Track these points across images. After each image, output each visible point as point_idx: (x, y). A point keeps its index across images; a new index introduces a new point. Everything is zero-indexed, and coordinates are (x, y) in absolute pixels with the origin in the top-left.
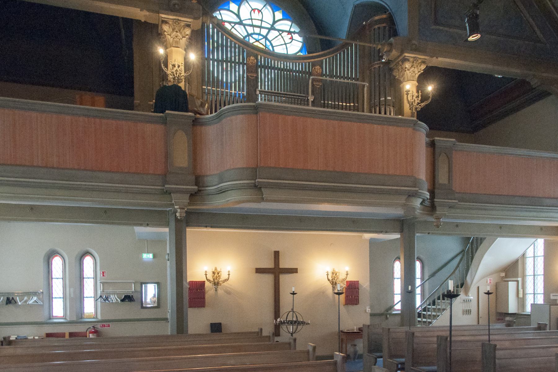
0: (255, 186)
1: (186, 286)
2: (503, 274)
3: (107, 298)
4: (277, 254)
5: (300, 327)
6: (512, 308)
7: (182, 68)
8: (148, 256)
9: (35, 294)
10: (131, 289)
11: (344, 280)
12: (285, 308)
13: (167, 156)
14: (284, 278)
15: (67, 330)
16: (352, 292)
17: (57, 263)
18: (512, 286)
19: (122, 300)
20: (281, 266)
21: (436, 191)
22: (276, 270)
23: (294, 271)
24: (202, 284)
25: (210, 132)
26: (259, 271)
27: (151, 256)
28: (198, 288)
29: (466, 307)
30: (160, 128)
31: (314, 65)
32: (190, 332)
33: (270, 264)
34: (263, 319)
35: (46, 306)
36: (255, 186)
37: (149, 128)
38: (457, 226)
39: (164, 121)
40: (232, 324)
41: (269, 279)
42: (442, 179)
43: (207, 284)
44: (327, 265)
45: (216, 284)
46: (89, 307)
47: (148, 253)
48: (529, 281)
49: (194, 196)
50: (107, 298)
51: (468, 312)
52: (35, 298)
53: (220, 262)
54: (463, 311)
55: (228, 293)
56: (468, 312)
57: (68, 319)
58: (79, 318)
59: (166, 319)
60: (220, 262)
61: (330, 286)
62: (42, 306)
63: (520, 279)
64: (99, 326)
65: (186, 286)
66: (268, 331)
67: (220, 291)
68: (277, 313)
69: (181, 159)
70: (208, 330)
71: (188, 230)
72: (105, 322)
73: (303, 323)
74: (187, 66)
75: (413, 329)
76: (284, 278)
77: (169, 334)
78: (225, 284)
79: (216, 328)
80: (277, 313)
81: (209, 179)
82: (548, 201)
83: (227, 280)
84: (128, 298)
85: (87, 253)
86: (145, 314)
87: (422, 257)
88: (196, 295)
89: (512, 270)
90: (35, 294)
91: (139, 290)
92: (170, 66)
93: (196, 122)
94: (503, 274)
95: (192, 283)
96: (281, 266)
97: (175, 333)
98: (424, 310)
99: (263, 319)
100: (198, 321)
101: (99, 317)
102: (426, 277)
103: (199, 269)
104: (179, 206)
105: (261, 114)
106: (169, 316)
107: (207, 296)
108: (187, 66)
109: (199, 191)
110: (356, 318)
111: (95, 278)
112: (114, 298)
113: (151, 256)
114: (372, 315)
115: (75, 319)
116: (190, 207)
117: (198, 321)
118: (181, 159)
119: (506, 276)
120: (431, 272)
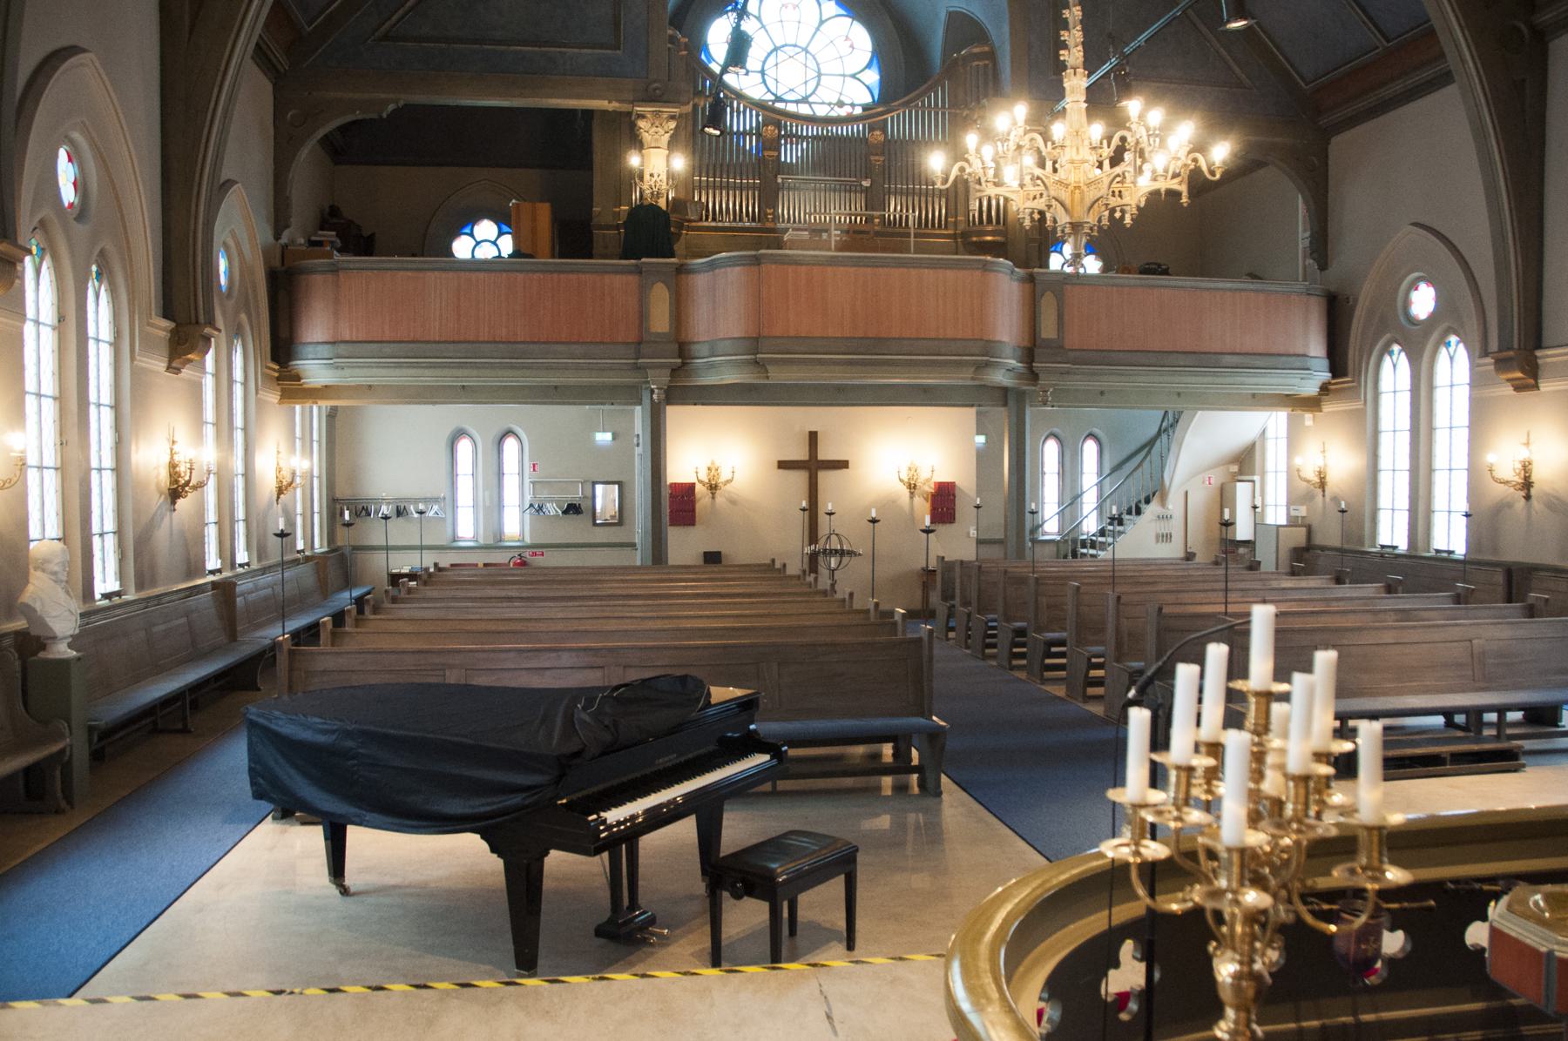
0: (756, 362)
1: (666, 493)
2: (1235, 468)
3: (540, 508)
4: (813, 437)
5: (846, 559)
6: (1243, 531)
7: (664, 177)
8: (603, 437)
9: (436, 500)
10: (577, 495)
11: (928, 480)
12: (823, 531)
13: (643, 316)
14: (825, 477)
15: (480, 559)
16: (944, 501)
17: (464, 447)
18: (1242, 491)
19: (565, 512)
20: (820, 457)
21: (1037, 351)
22: (813, 465)
23: (843, 465)
24: (692, 486)
25: (700, 281)
26: (783, 465)
27: (608, 436)
28: (685, 493)
29: (1163, 528)
30: (633, 279)
31: (872, 129)
32: (670, 562)
33: (801, 454)
34: (789, 547)
35: (449, 521)
36: (756, 362)
37: (618, 281)
38: (1102, 393)
39: (638, 271)
40: (739, 552)
41: (799, 478)
42: (1048, 330)
43: (699, 488)
44: (903, 455)
45: (713, 488)
46: (514, 525)
47: (604, 431)
48: (1270, 478)
49: (675, 371)
50: (540, 508)
51: (1167, 537)
52: (436, 508)
53: (721, 451)
54: (1157, 537)
55: (733, 502)
56: (1167, 537)
57: (482, 542)
58: (497, 545)
59: (633, 545)
60: (721, 451)
61: (906, 492)
62: (444, 519)
63: (1256, 478)
64: (527, 554)
65: (666, 493)
66: (794, 568)
67: (719, 499)
68: (813, 537)
69: (660, 321)
70: (700, 561)
71: (669, 408)
72: (539, 548)
73: (851, 553)
74: (671, 176)
75: (1530, 601)
76: (825, 477)
77: (638, 563)
78: (728, 487)
79: (712, 558)
80: (813, 537)
81: (697, 347)
82: (1228, 359)
83: (728, 481)
84: (573, 509)
85: (509, 432)
86: (601, 536)
87: (1096, 431)
88: (680, 505)
89: (1245, 461)
90: (436, 500)
91: (589, 494)
92: (647, 177)
93: (681, 270)
94: (1235, 468)
95: (674, 486)
96: (820, 457)
97: (649, 563)
98: (1102, 533)
99: (789, 547)
100: (684, 546)
101: (528, 540)
102: (1107, 471)
103: (683, 465)
104: (657, 382)
105: (764, 267)
106: (637, 540)
107: (698, 506)
108: (671, 176)
109: (684, 364)
110: (958, 543)
111: (521, 474)
112: (552, 509)
113: (608, 436)
114: (980, 542)
115: (491, 542)
116: (672, 376)
117: (684, 546)
118: (660, 321)
119: (1241, 472)
120: (1116, 462)
